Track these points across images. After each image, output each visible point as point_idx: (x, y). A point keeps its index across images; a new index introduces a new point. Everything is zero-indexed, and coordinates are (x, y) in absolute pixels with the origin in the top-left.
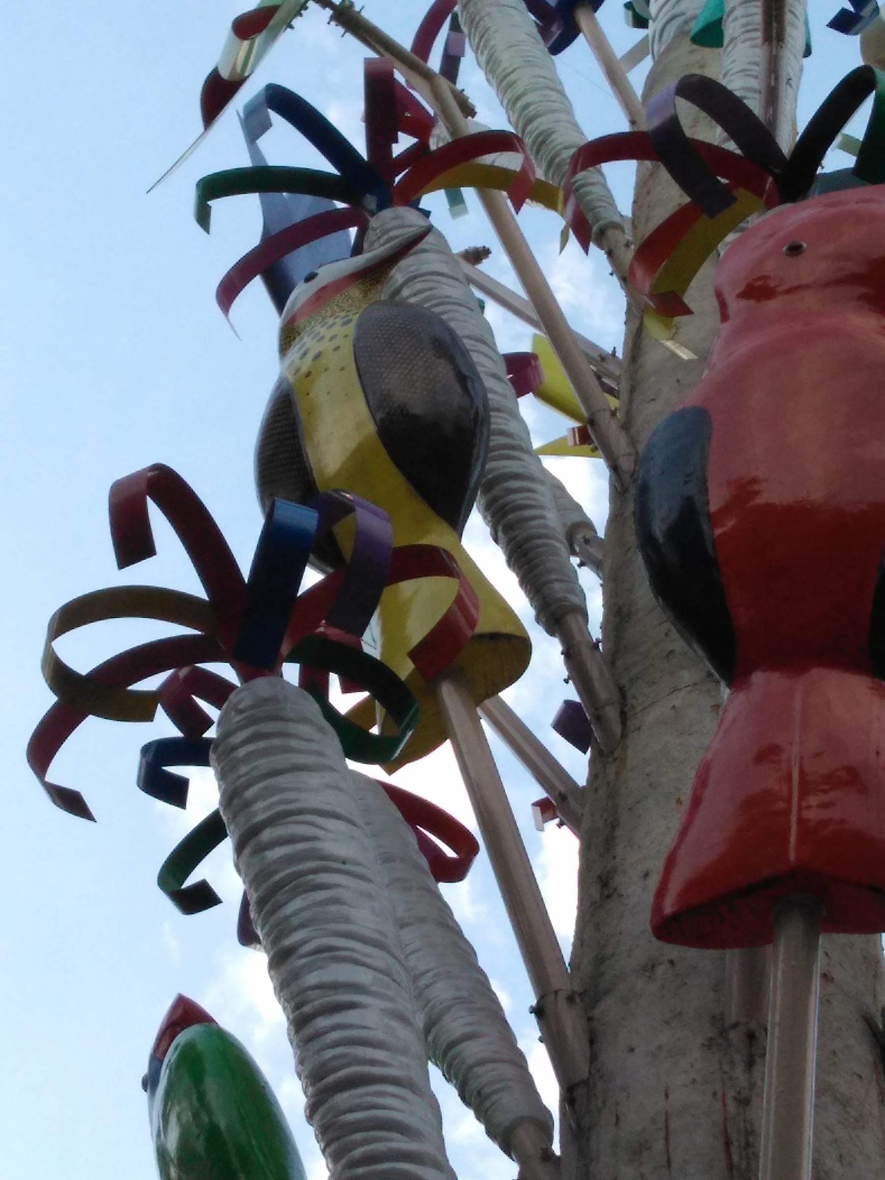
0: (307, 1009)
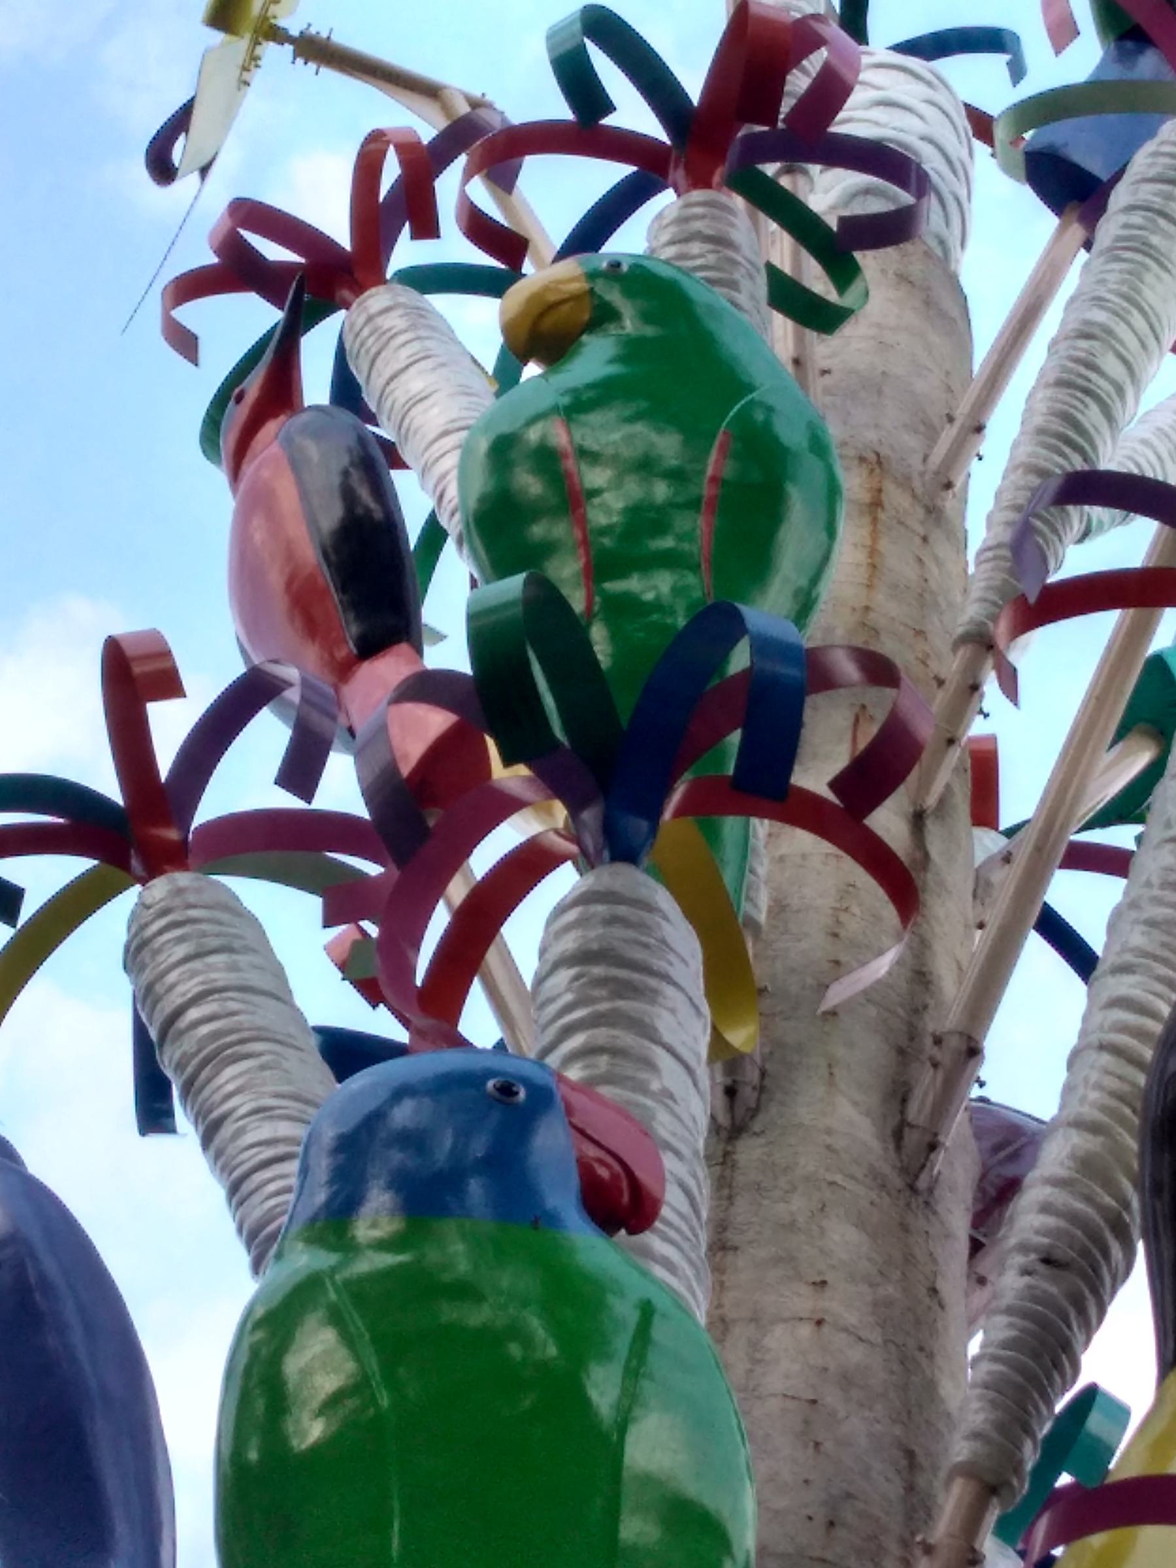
0: (237, 1173)
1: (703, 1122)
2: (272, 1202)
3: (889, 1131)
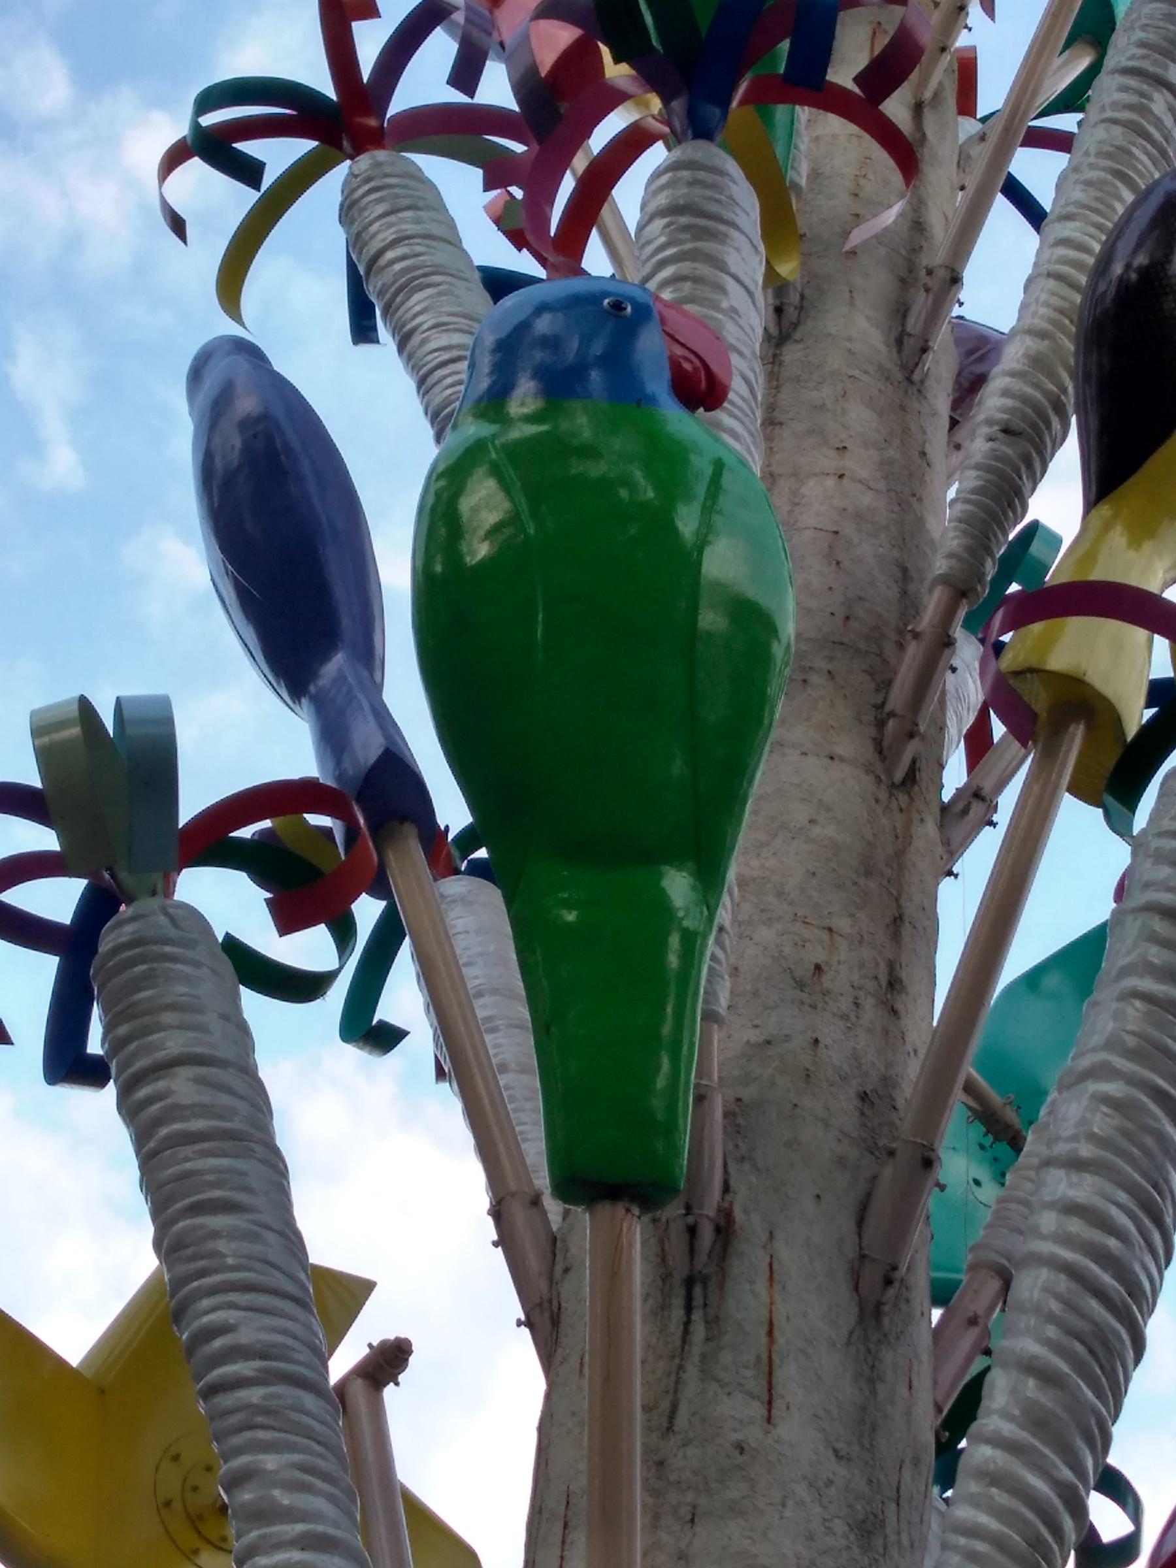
1: (760, 332)
2: (449, 392)
3: (892, 339)
